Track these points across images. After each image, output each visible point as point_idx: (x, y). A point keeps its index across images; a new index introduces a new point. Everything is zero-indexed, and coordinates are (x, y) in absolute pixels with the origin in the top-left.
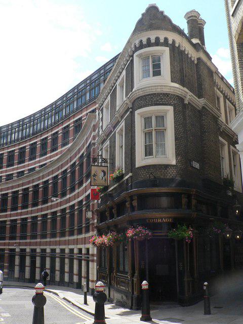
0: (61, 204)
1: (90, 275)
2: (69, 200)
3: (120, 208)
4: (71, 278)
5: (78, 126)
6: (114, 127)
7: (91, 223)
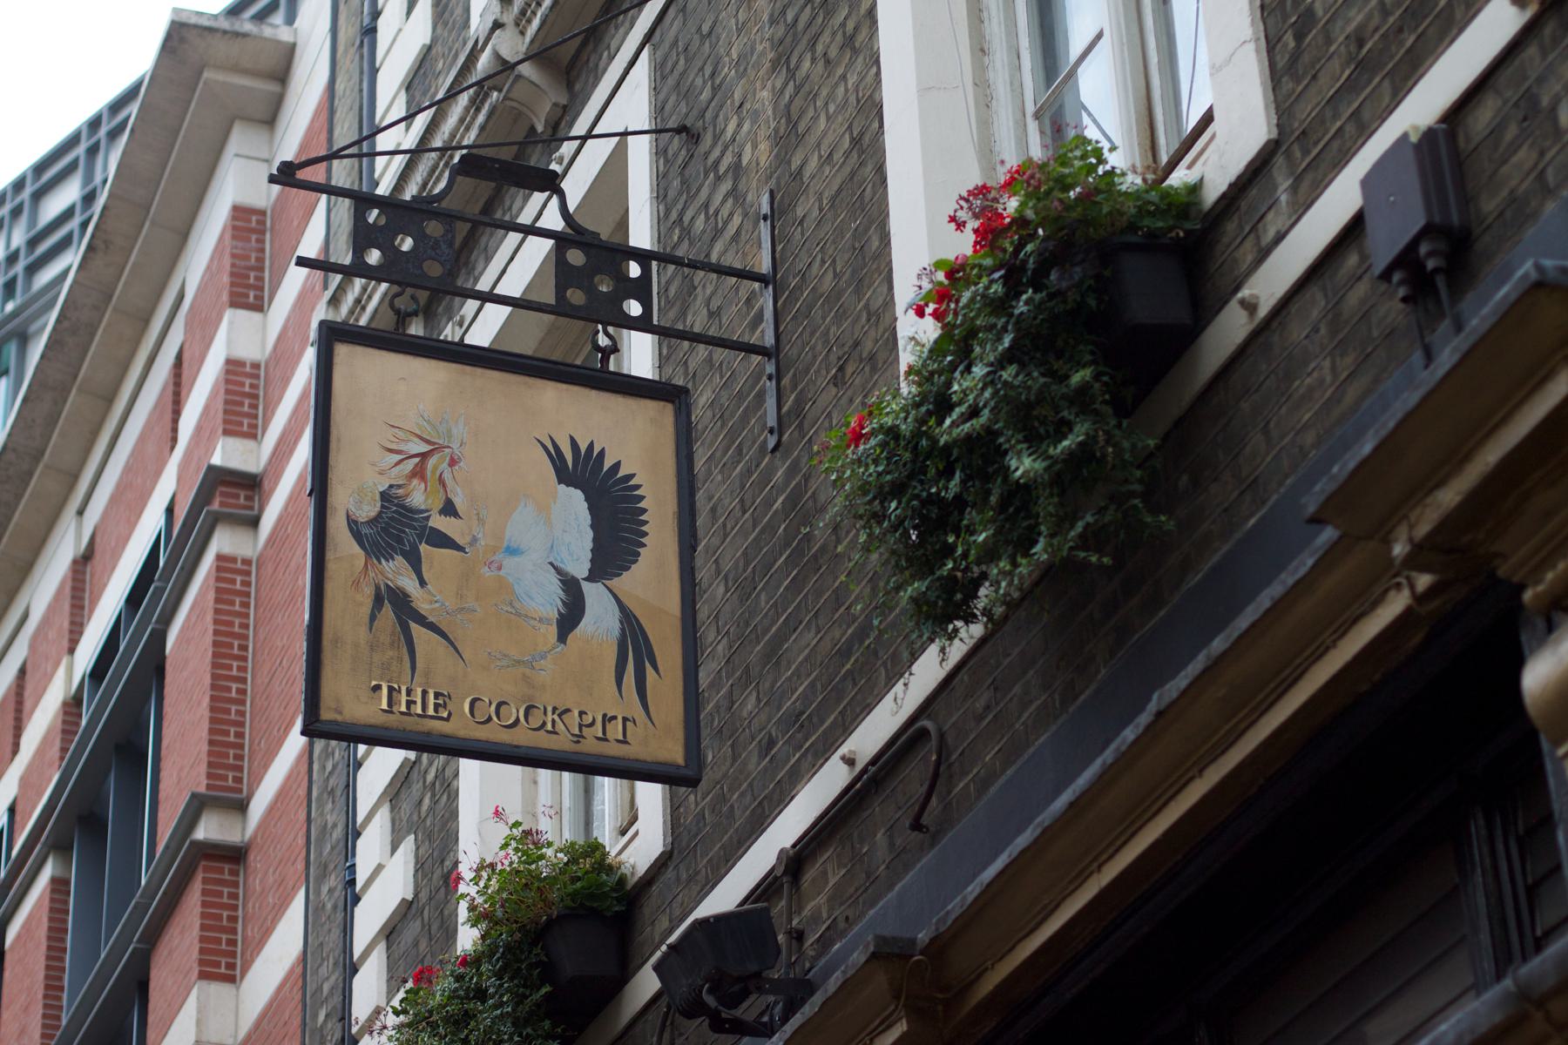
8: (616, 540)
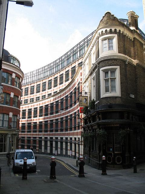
0: (65, 114)
1: (80, 152)
3: (94, 118)
4: (51, 150)
5: (74, 70)
7: (80, 124)
8: (86, 100)
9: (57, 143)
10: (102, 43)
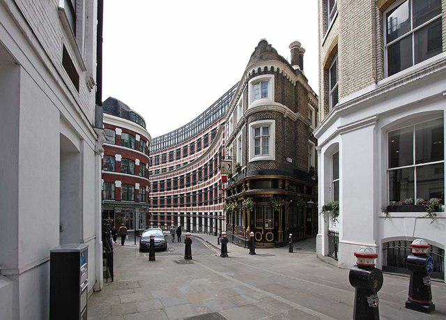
2: (209, 183)
3: (239, 188)
6: (235, 135)
9: (195, 219)
10: (253, 88)
